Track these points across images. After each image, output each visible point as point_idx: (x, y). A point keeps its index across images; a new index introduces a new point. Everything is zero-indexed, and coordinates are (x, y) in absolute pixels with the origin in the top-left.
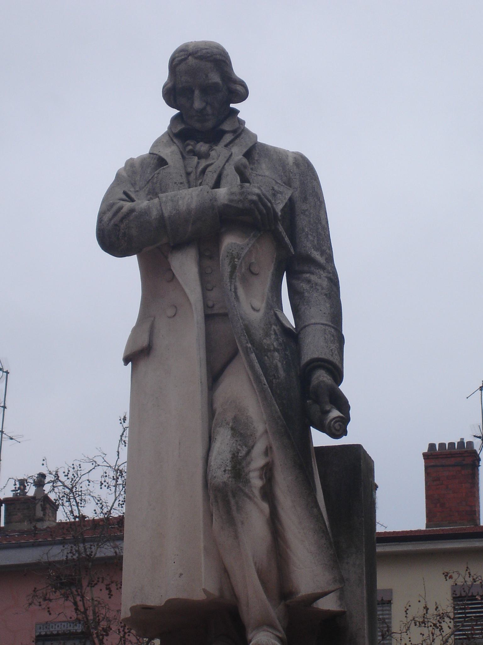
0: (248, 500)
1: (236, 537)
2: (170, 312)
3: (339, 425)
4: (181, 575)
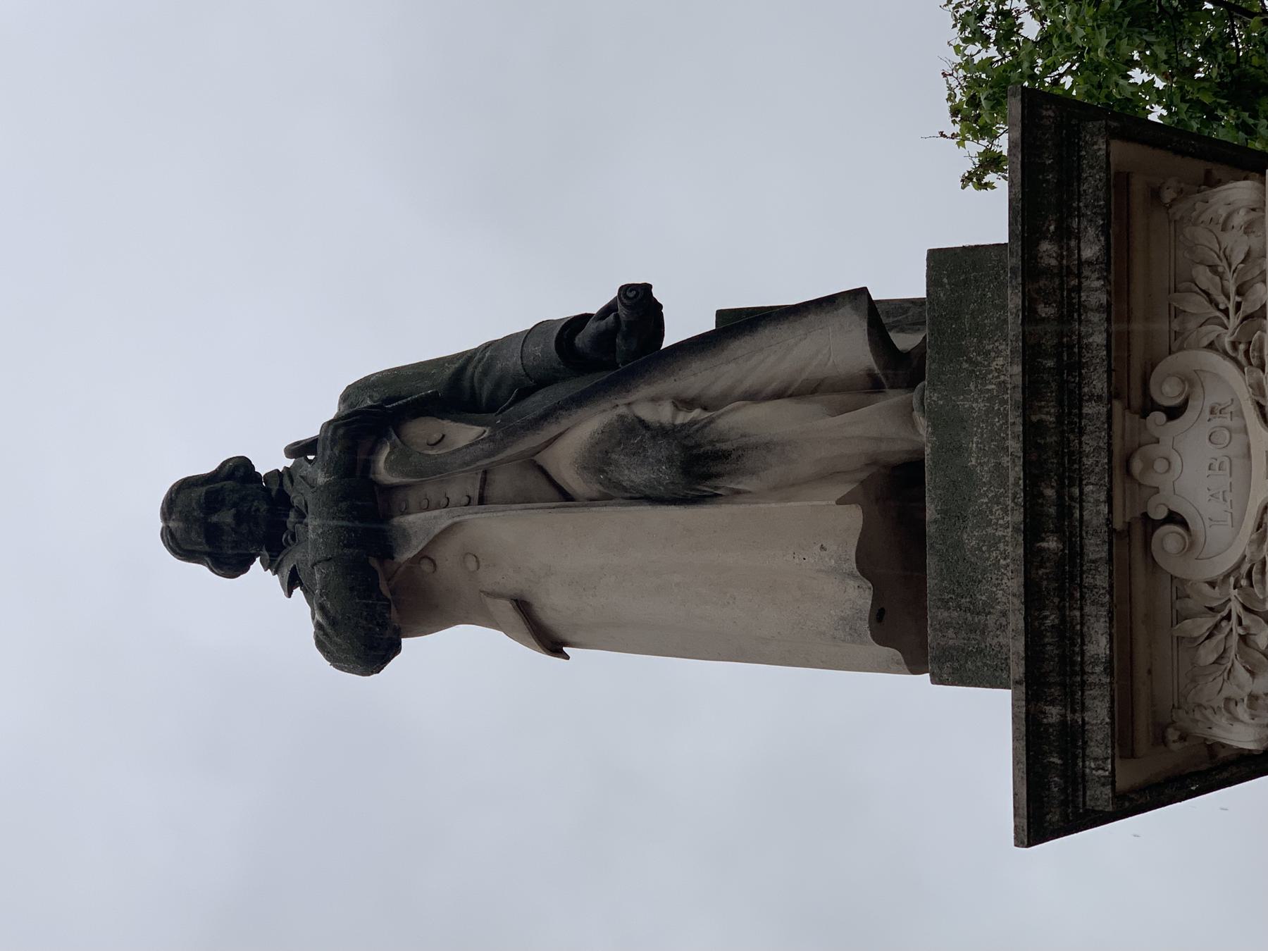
0: (712, 425)
1: (768, 446)
2: (472, 565)
3: (631, 291)
4: (822, 548)
